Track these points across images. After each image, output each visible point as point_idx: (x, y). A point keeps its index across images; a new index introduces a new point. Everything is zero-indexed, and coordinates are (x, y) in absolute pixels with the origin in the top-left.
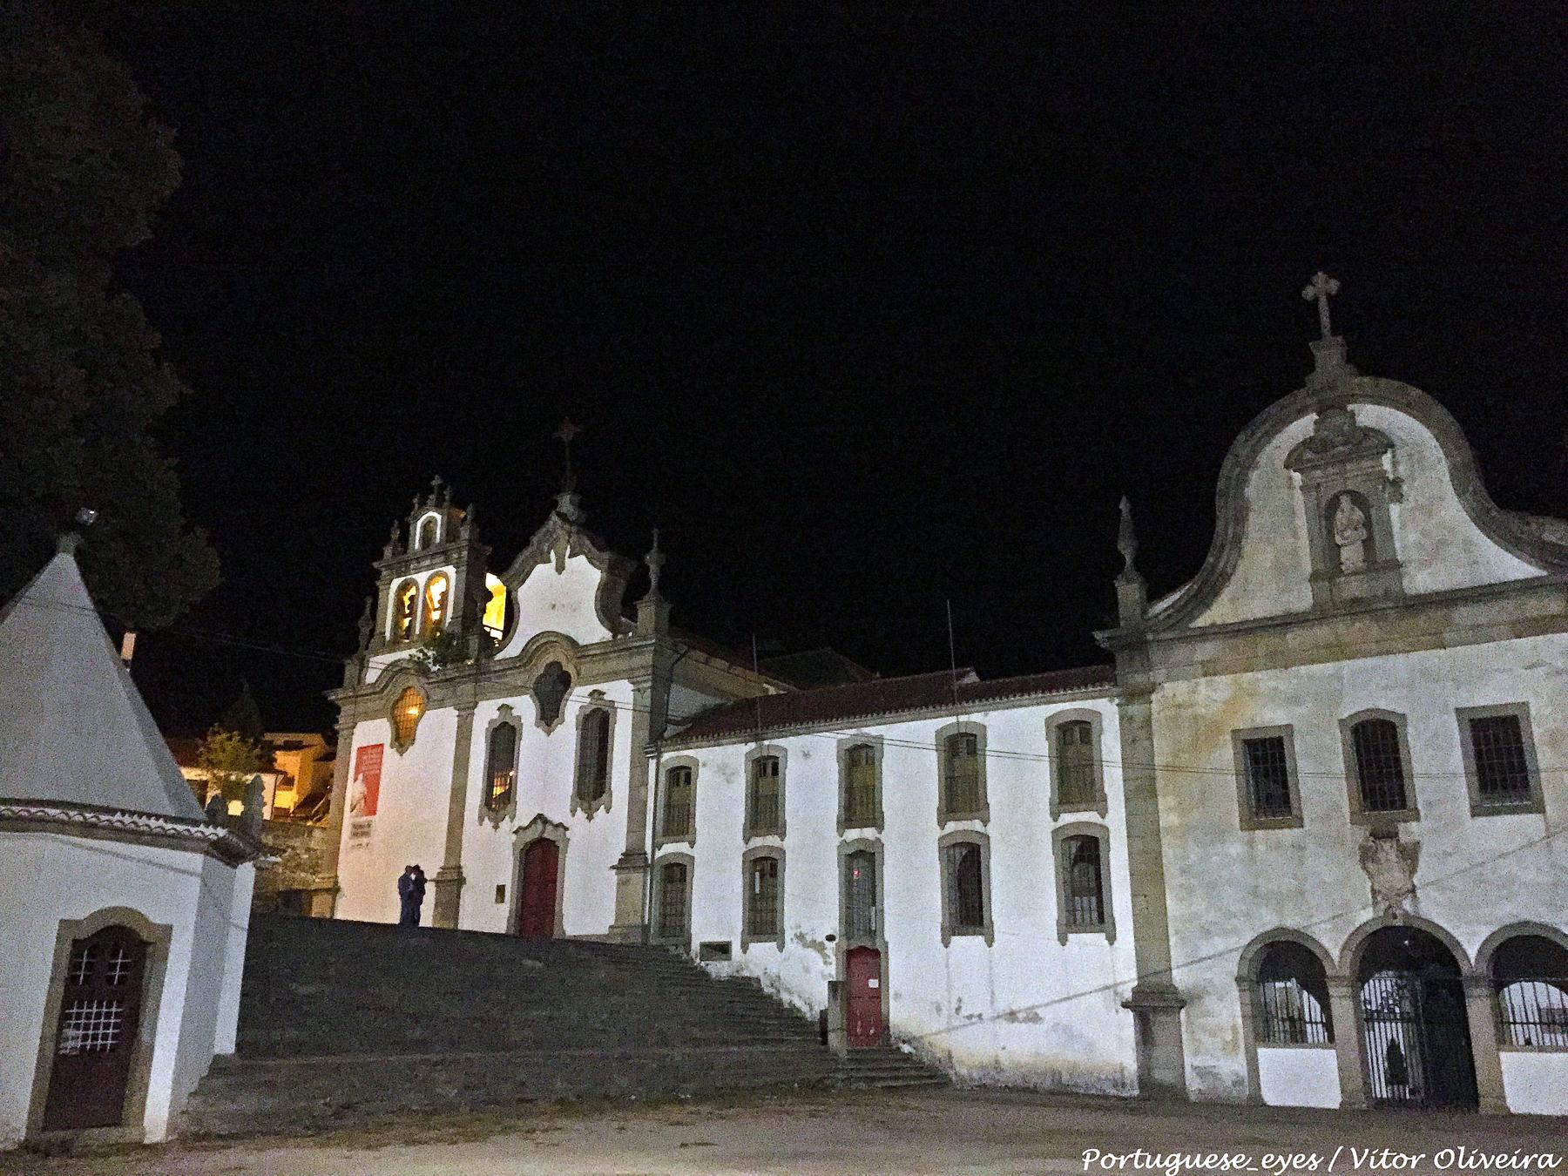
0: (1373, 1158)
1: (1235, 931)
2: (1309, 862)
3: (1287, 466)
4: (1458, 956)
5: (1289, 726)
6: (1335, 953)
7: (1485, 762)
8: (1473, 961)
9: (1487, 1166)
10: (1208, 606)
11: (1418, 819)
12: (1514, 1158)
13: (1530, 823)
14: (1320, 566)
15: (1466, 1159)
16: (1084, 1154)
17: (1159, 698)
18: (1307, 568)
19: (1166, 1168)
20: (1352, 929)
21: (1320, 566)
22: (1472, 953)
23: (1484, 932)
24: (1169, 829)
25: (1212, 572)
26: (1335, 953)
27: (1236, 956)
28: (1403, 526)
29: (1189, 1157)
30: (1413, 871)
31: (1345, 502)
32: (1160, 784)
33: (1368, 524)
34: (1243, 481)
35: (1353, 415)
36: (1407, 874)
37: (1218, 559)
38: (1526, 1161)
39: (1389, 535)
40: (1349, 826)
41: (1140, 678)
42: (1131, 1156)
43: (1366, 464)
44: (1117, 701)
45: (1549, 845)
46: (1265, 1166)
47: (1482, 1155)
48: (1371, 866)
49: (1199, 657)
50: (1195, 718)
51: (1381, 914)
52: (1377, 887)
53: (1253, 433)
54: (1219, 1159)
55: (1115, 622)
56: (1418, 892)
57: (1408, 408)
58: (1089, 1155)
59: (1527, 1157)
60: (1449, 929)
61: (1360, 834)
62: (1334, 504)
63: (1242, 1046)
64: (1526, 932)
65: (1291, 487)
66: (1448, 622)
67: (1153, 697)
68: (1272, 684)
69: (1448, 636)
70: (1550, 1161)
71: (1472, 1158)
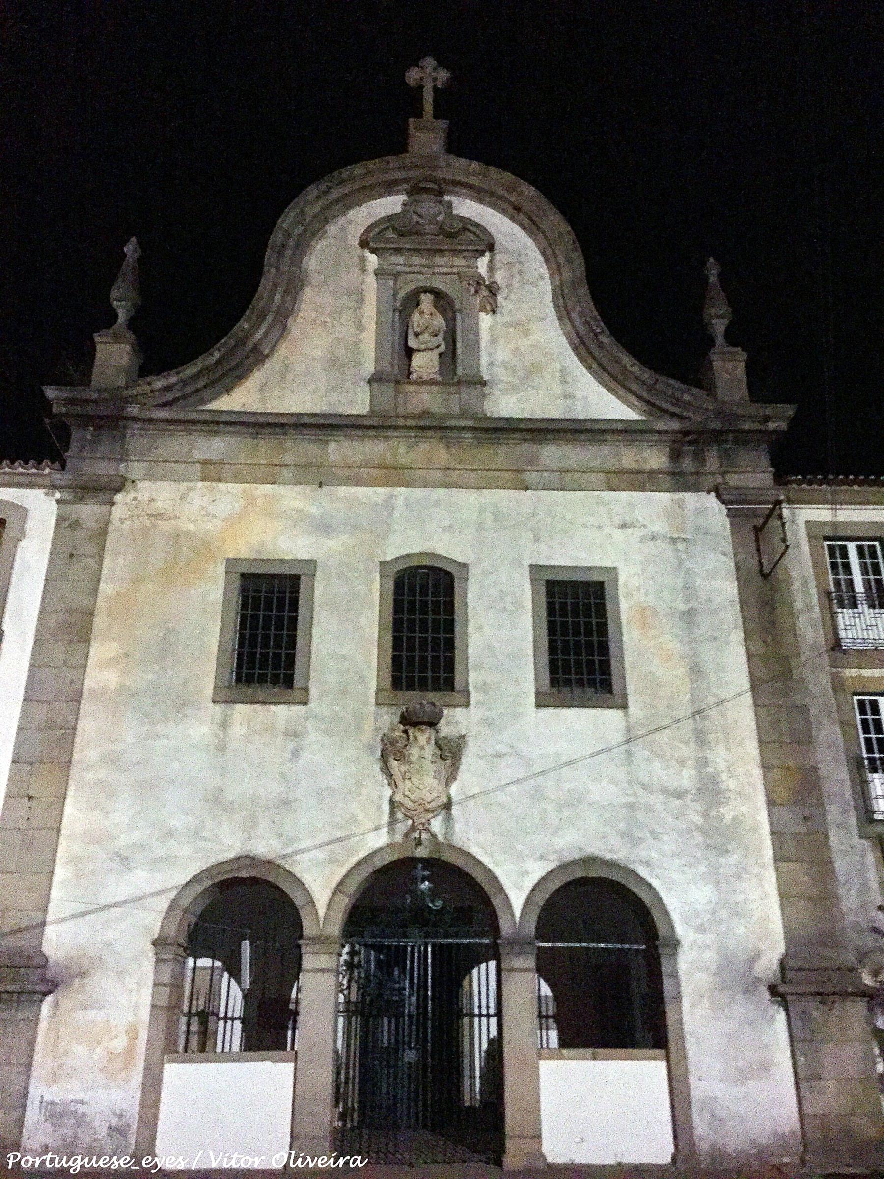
0: (226, 1160)
1: (171, 860)
2: (306, 756)
3: (364, 244)
4: (496, 902)
5: (312, 563)
6: (321, 899)
7: (559, 638)
8: (518, 912)
9: (311, 1165)
10: (228, 390)
11: (467, 705)
12: (332, 1160)
13: (611, 718)
14: (387, 367)
15: (295, 1161)
16: (8, 1156)
17: (128, 501)
18: (369, 368)
19: (70, 1167)
20: (354, 860)
21: (387, 367)
22: (517, 901)
23: (537, 871)
24: (100, 694)
25: (243, 342)
26: (321, 899)
27: (163, 903)
28: (493, 341)
29: (87, 1158)
30: (451, 778)
31: (427, 301)
32: (99, 622)
33: (451, 337)
34: (302, 248)
35: (450, 205)
36: (443, 780)
37: (257, 326)
38: (341, 1161)
39: (475, 347)
40: (372, 708)
41: (103, 469)
42: (44, 1158)
43: (459, 262)
44: (58, 495)
45: (629, 753)
46: (145, 1166)
47: (308, 1157)
48: (394, 764)
49: (198, 455)
50: (176, 537)
51: (398, 838)
52: (398, 798)
53: (327, 192)
54: (110, 1160)
55: (85, 378)
56: (455, 811)
57: (515, 211)
58: (12, 1157)
59: (342, 1158)
60: (491, 866)
61: (389, 718)
62: (412, 301)
63: (141, 1064)
64: (594, 873)
65: (364, 270)
66: (533, 460)
67: (119, 497)
68: (298, 504)
69: (532, 477)
70: (358, 1162)
71: (300, 1160)
